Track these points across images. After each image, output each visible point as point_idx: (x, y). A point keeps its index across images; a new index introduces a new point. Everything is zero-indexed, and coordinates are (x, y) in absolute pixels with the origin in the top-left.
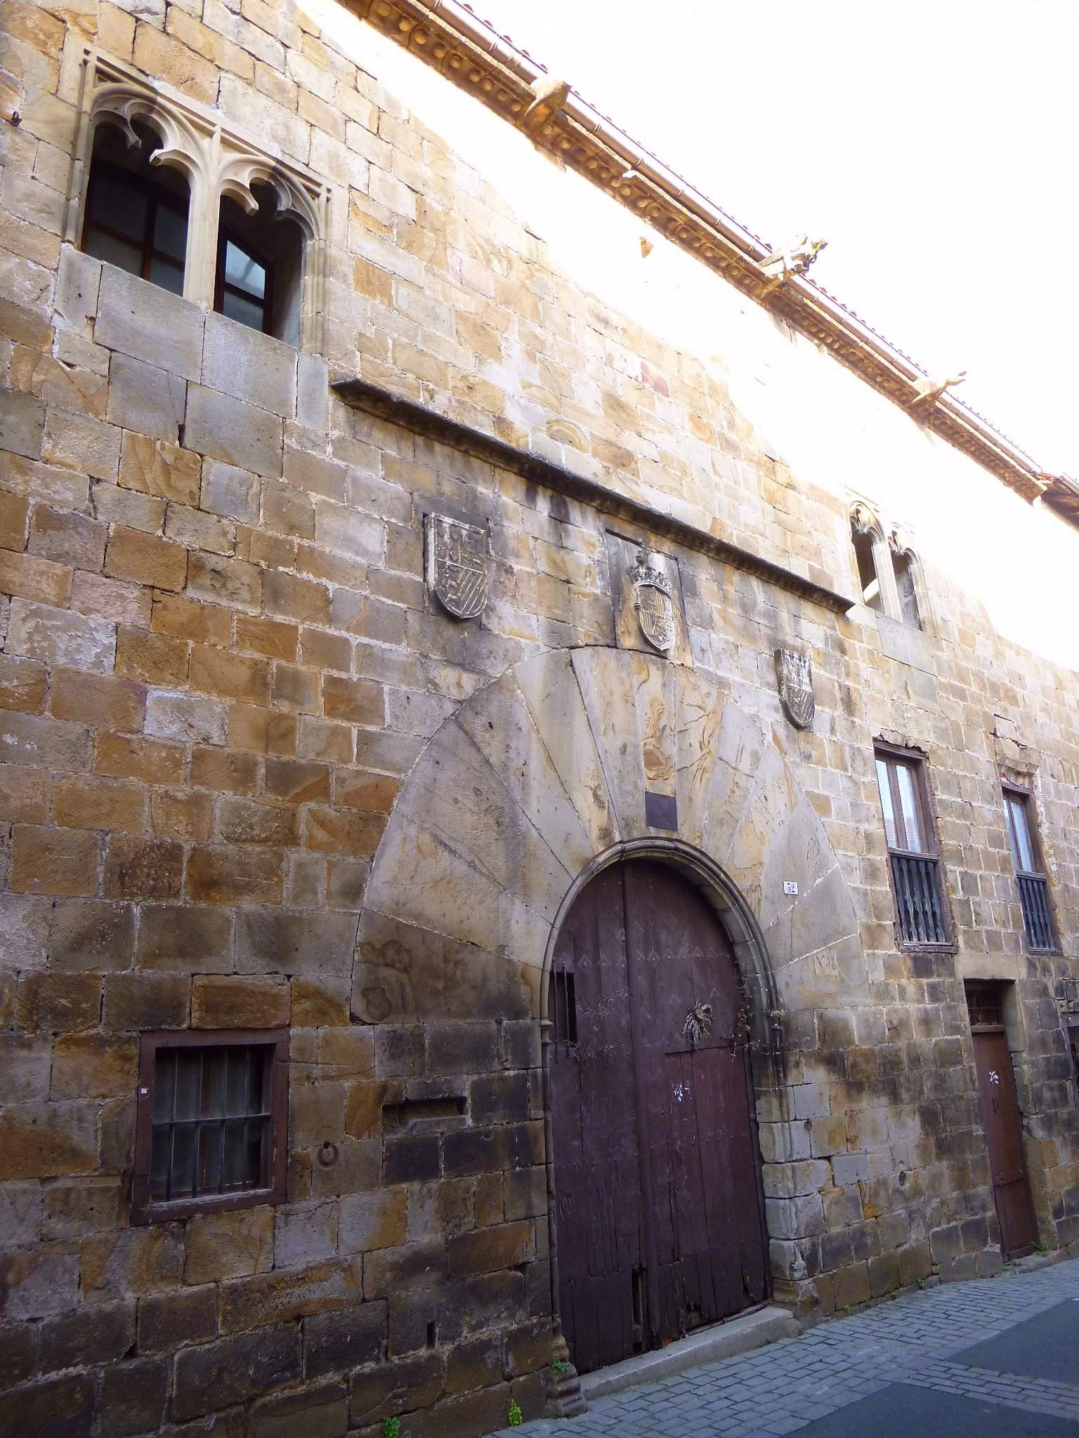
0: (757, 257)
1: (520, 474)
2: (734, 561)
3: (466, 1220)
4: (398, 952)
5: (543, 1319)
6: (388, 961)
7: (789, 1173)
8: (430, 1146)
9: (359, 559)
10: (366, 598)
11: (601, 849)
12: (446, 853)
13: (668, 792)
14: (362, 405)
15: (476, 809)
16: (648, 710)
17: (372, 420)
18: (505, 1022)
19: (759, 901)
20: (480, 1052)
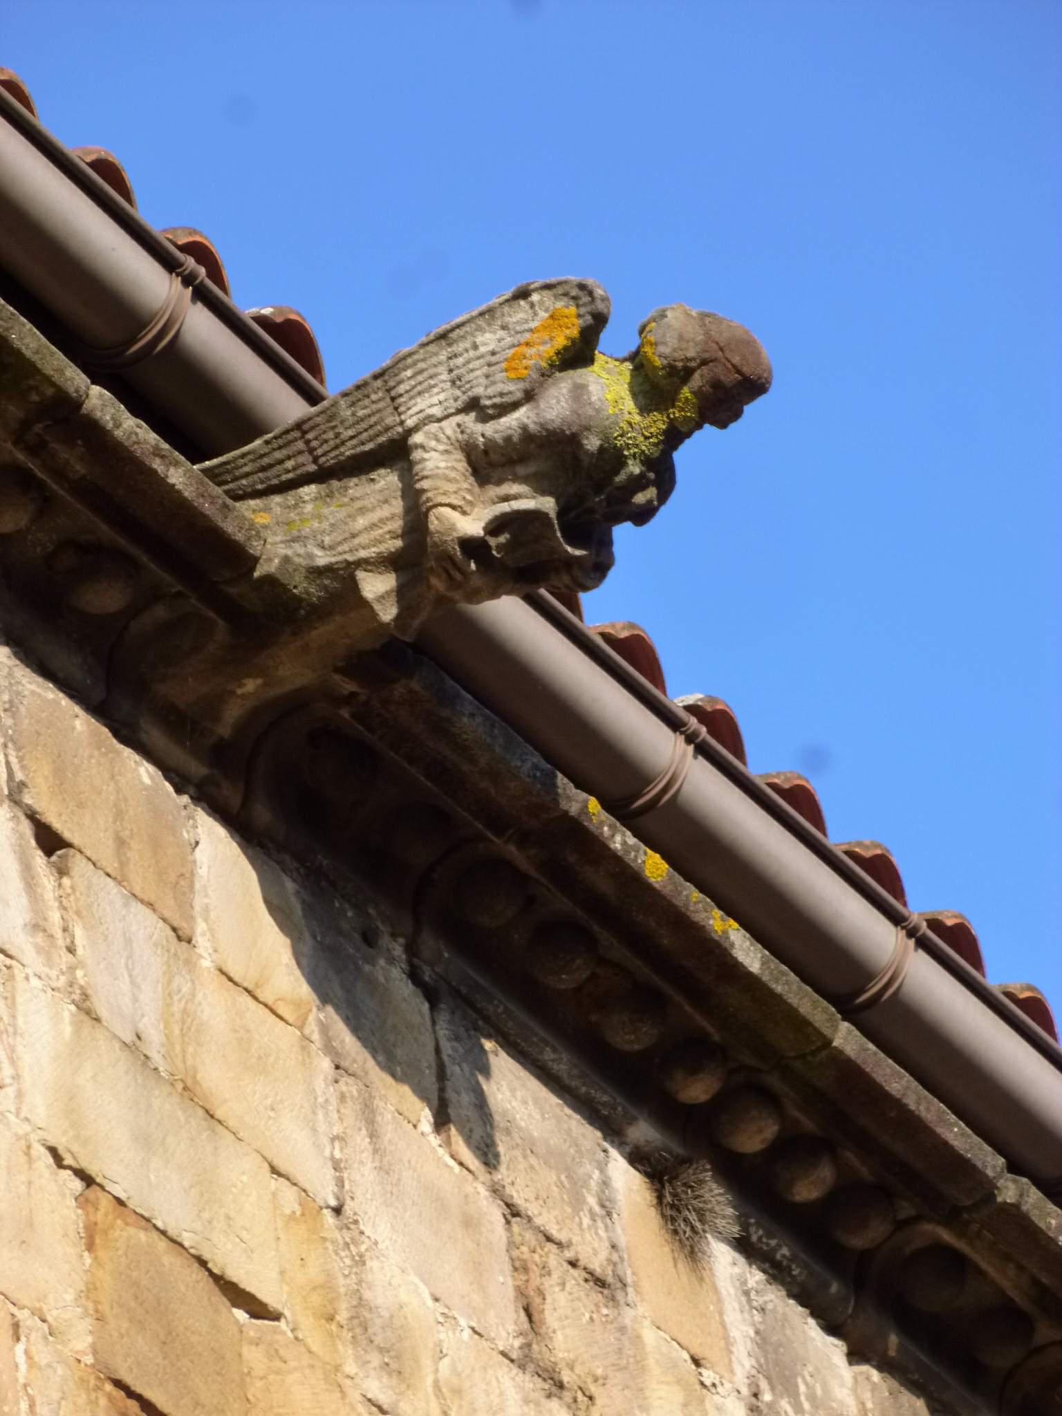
0: (200, 415)
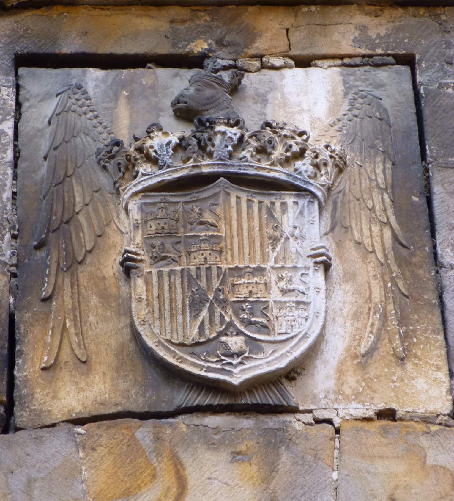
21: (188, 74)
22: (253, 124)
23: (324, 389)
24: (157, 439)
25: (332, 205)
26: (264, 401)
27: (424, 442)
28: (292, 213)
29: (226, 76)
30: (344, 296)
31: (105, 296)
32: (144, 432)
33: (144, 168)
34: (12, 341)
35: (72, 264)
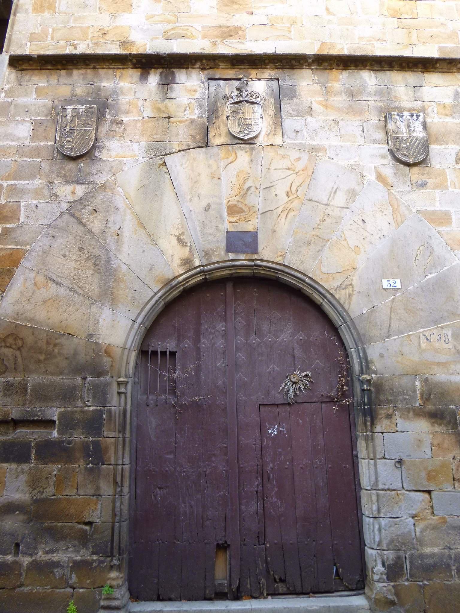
1: (135, 67)
2: (338, 65)
3: (47, 490)
4: (15, 340)
5: (102, 559)
6: (8, 345)
7: (374, 498)
8: (26, 446)
9: (13, 143)
10: (16, 161)
11: (181, 272)
12: (54, 285)
13: (249, 227)
14: (24, 67)
15: (79, 259)
16: (234, 180)
17: (31, 72)
18: (89, 378)
19: (350, 296)
20: (68, 395)
21: (238, 82)
22: (250, 92)
23: (260, 140)
24: (232, 149)
25: (263, 106)
26: (250, 142)
27: (278, 149)
28: (256, 108)
29: (245, 82)
30: (265, 124)
31: (223, 123)
32: (230, 147)
33: (231, 99)
34: (208, 131)
35: (218, 117)
